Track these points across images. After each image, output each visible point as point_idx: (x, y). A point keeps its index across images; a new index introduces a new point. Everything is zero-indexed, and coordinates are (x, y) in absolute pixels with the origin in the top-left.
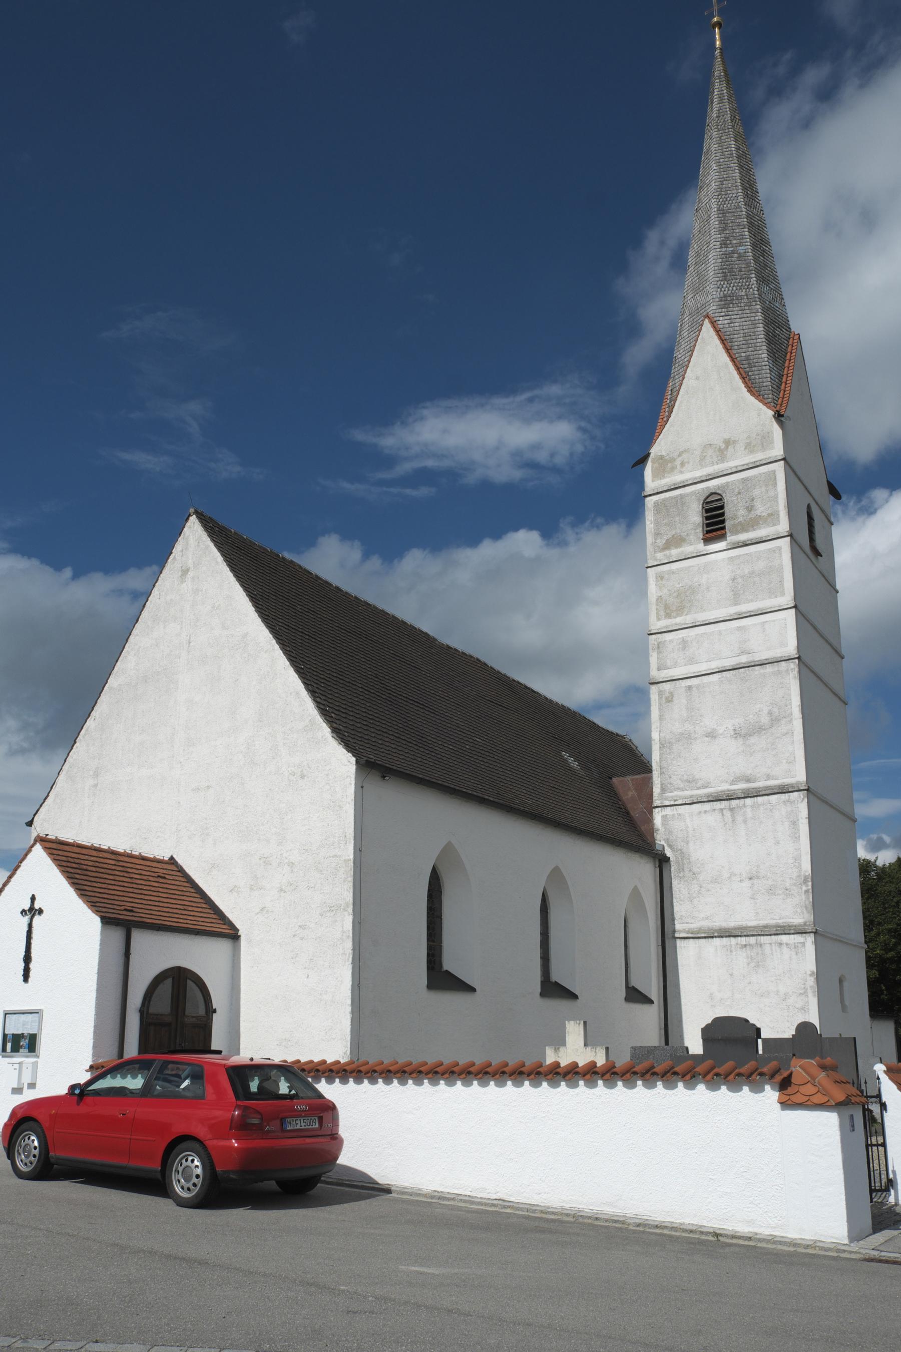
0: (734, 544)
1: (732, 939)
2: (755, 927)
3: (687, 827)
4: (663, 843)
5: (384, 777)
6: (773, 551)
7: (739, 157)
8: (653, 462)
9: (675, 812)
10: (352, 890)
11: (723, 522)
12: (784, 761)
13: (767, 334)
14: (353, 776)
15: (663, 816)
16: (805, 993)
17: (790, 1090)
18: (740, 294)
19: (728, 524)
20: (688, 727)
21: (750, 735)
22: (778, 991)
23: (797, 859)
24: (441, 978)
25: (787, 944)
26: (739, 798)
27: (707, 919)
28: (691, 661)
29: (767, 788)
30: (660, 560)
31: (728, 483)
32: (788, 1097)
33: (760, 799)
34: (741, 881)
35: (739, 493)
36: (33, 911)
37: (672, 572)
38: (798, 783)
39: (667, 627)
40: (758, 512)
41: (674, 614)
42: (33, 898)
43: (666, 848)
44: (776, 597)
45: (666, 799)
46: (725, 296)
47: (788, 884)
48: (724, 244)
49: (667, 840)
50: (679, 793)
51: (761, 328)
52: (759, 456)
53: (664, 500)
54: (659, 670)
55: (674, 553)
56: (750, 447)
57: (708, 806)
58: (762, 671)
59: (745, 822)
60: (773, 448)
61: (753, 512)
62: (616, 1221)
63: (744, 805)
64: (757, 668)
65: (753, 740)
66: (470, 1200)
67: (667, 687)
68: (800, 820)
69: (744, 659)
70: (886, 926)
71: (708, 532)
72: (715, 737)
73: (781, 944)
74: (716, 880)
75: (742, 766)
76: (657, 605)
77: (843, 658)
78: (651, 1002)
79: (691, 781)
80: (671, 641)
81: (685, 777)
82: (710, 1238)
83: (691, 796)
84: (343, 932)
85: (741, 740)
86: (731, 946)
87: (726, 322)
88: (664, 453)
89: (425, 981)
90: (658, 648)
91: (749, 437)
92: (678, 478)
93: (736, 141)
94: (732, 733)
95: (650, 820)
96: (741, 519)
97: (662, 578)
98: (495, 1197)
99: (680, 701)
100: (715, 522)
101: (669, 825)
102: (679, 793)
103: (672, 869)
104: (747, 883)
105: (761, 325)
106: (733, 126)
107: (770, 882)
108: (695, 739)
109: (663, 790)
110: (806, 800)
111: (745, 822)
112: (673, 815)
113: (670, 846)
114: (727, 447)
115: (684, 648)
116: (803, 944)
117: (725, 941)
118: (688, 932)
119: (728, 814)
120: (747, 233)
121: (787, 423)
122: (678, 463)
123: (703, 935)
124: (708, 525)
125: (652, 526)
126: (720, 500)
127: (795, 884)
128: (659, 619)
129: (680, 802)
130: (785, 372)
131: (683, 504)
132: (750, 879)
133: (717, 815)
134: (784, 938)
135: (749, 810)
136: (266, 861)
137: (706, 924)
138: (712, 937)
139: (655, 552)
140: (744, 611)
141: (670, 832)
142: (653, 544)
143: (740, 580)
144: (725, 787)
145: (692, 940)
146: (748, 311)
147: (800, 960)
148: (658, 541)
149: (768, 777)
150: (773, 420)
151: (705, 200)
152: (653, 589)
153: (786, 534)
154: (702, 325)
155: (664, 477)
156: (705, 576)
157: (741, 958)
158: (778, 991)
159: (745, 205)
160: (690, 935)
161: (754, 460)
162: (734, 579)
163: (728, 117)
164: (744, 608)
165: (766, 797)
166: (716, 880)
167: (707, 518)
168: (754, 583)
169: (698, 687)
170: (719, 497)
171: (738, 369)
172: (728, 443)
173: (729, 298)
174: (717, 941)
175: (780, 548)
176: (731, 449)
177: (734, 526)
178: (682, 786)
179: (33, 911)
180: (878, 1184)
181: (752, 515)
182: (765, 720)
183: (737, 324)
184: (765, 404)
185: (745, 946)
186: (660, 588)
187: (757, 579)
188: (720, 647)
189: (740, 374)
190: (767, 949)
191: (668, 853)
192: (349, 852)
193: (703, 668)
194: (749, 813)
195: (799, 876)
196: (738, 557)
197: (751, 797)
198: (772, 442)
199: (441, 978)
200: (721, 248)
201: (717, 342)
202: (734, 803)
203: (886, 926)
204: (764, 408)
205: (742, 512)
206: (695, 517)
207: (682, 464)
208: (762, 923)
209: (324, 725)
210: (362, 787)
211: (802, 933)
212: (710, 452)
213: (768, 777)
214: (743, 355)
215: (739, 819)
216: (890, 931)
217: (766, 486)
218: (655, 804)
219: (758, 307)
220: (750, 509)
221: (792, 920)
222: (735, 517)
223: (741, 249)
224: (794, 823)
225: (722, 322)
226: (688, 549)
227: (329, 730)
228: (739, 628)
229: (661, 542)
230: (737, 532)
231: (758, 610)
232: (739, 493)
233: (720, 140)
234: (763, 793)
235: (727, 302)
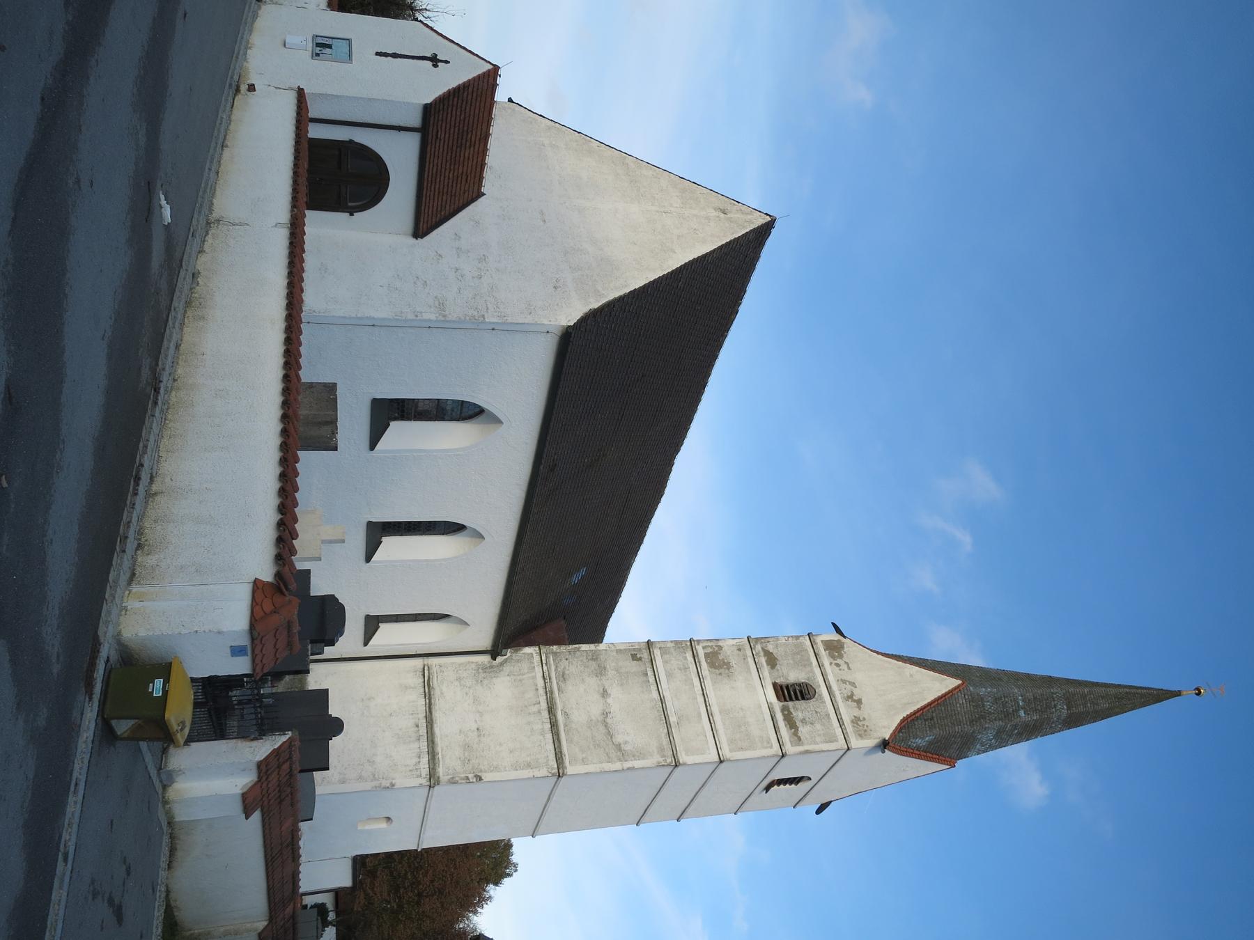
6: (769, 741)
11: (791, 699)
19: (790, 704)
20: (611, 673)
23: (497, 769)
24: (378, 532)
28: (669, 675)
36: (434, 60)
42: (446, 62)
50: (553, 668)
56: (856, 721)
69: (673, 719)
75: (578, 717)
79: (563, 677)
80: (685, 658)
82: (146, 373)
92: (826, 661)
95: (530, 644)
99: (634, 666)
102: (553, 668)
104: (474, 727)
109: (555, 654)
111: (529, 723)
113: (506, 661)
119: (535, 709)
122: (839, 661)
134: (425, 759)
136: (483, 259)
144: (559, 706)
172: (859, 702)
179: (434, 60)
181: (799, 724)
182: (619, 738)
190: (416, 745)
191: (499, 659)
199: (378, 532)
202: (546, 714)
205: (800, 715)
206: (793, 676)
207: (838, 665)
220: (803, 721)
223: (1022, 713)
226: (766, 670)
228: (699, 715)
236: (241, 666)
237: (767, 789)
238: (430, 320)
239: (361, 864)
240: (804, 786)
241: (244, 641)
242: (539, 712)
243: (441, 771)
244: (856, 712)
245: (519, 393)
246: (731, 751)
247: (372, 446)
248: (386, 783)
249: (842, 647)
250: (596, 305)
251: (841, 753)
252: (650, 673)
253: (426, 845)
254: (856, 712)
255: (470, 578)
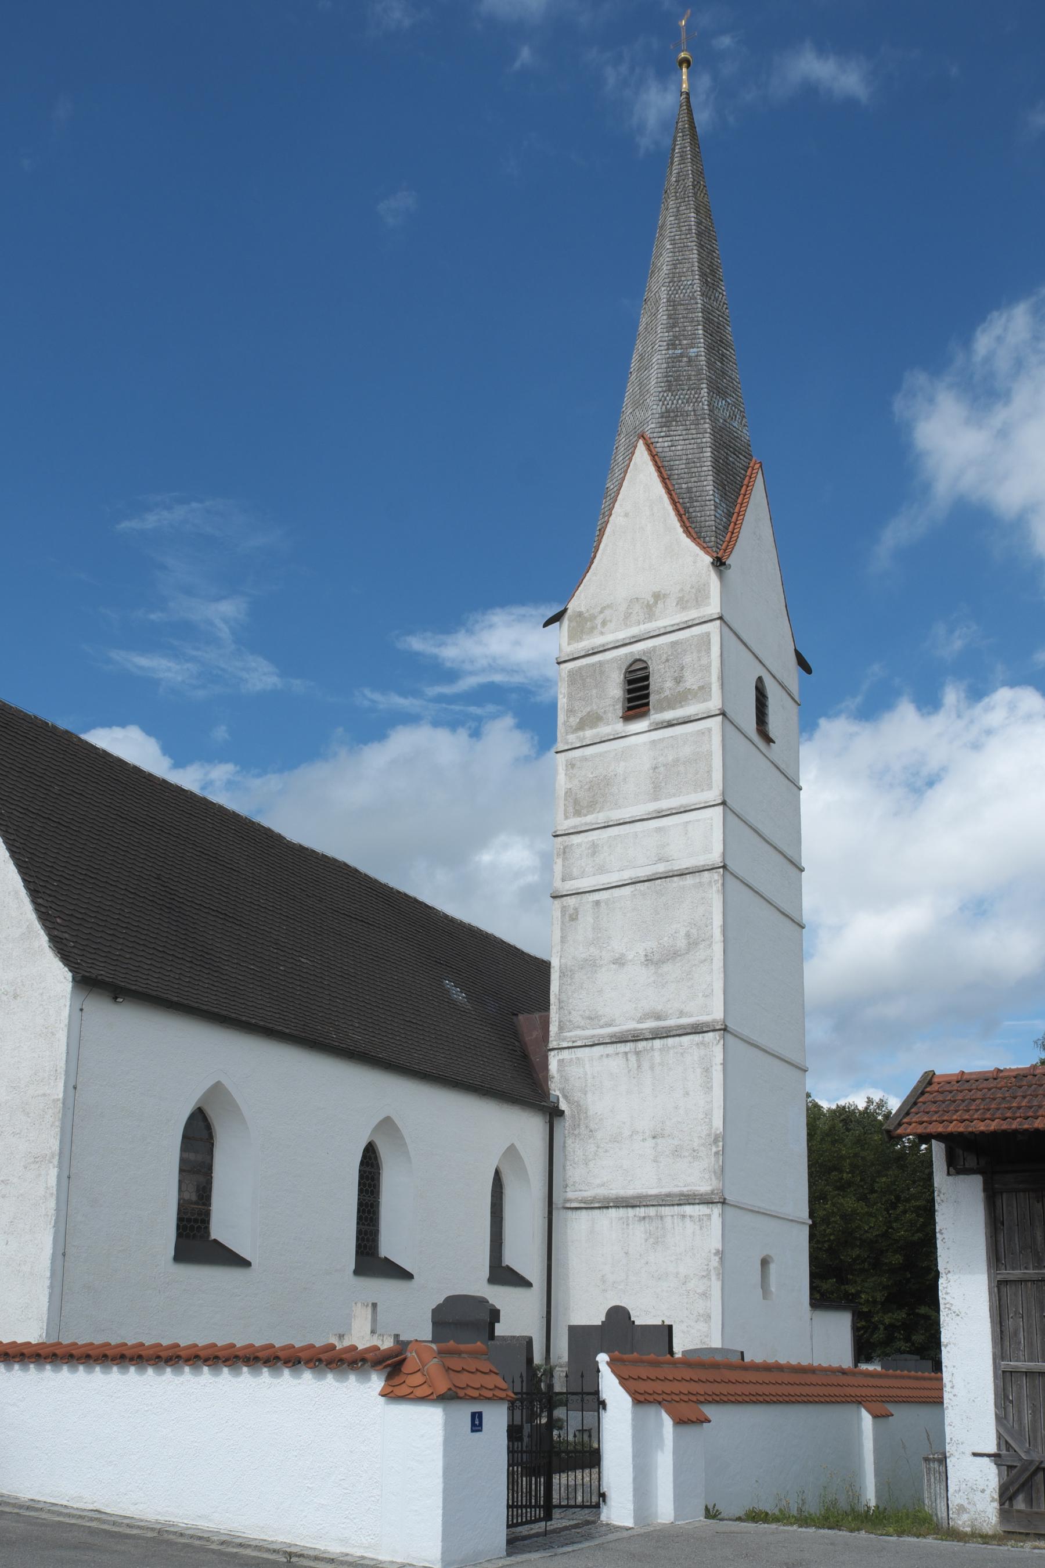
0: (657, 724)
1: (630, 1210)
2: (656, 1196)
3: (586, 1074)
4: (557, 1093)
5: (115, 998)
6: (701, 733)
7: (699, 234)
8: (570, 621)
9: (573, 1056)
10: (58, 1137)
11: (647, 696)
12: (701, 995)
13: (716, 460)
14: (69, 996)
15: (559, 1061)
16: (707, 1276)
17: (397, 1380)
18: (686, 409)
19: (653, 699)
21: (663, 962)
22: (677, 1273)
23: (708, 1114)
25: (691, 1217)
26: (647, 1039)
27: (603, 1185)
28: (602, 870)
29: (679, 1027)
30: (572, 743)
31: (655, 647)
32: (391, 1389)
33: (670, 1041)
34: (644, 1140)
35: (667, 660)
37: (585, 759)
38: (715, 1021)
39: (575, 827)
40: (688, 685)
41: (584, 811)
43: (561, 1099)
44: (702, 790)
45: (564, 1040)
46: (668, 411)
47: (695, 1144)
48: (672, 345)
49: (562, 1090)
50: (579, 1032)
51: (708, 453)
52: (693, 614)
53: (580, 668)
54: (563, 880)
55: (589, 734)
56: (682, 603)
57: (610, 1049)
58: (681, 883)
59: (652, 1068)
60: (709, 604)
61: (681, 684)
62: (200, 1538)
63: (652, 1049)
64: (675, 878)
65: (666, 968)
66: (52, 1509)
67: (571, 901)
68: (714, 1067)
69: (661, 868)
70: (914, 1203)
71: (630, 709)
72: (623, 964)
73: (684, 1216)
74: (615, 1139)
76: (565, 800)
77: (802, 870)
78: (527, 1284)
79: (593, 1019)
80: (579, 845)
81: (587, 1013)
83: (593, 1036)
84: (47, 1188)
85: (652, 968)
86: (628, 1218)
87: (666, 444)
88: (583, 609)
89: (352, 1266)
90: (564, 852)
91: (682, 590)
93: (697, 212)
94: (643, 959)
96: (667, 693)
97: (573, 766)
98: (91, 1507)
99: (587, 919)
100: (638, 695)
101: (568, 1069)
102: (579, 1032)
103: (567, 1124)
104: (650, 1142)
105: (709, 449)
106: (695, 194)
107: (676, 1142)
108: (601, 966)
109: (561, 1028)
110: (722, 1042)
111: (652, 1068)
112: (571, 1059)
113: (565, 1097)
114: (656, 603)
115: (594, 854)
116: (709, 1216)
117: (622, 1212)
118: (581, 1201)
119: (633, 1058)
120: (701, 332)
121: (730, 573)
122: (599, 621)
123: (597, 1205)
124: (630, 700)
125: (565, 700)
126: (646, 668)
127: (703, 1145)
128: (566, 818)
129: (579, 1043)
130: (737, 510)
131: (602, 673)
132: (654, 1138)
133: (620, 1061)
134: (688, 1209)
135: (656, 1054)
137: (602, 1192)
138: (607, 1207)
139: (567, 734)
140: (664, 808)
141: (567, 1080)
142: (564, 723)
143: (662, 769)
144: (632, 1025)
145: (584, 1212)
146: (694, 432)
147: (700, 1235)
148: (571, 719)
149: (682, 1014)
150: (711, 568)
151: (654, 289)
152: (562, 782)
153: (718, 712)
154: (635, 447)
155: (581, 639)
156: (622, 764)
157: (639, 1232)
158: (677, 1273)
159: (703, 295)
160: (583, 1205)
161: (686, 619)
162: (655, 768)
163: (689, 182)
164: (665, 804)
165: (677, 1039)
166: (615, 1139)
167: (629, 691)
168: (678, 773)
169: (607, 902)
170: (645, 665)
171: (674, 503)
172: (657, 597)
173: (672, 414)
174: (612, 1212)
175: (710, 730)
176: (660, 605)
177: (659, 701)
178: (582, 1024)
180: (579, 1499)
181: (681, 688)
182: (681, 943)
183: (679, 448)
184: (703, 548)
185: (644, 1218)
186: (570, 777)
187: (682, 768)
188: (631, 853)
189: (676, 509)
190: (668, 1221)
191: (563, 1106)
192: (58, 1090)
193: (614, 878)
194: (657, 1057)
195: (709, 1135)
196: (662, 740)
197: (660, 1038)
198: (708, 597)
200: (668, 349)
201: (651, 468)
202: (641, 1045)
203: (914, 1203)
204: (701, 553)
205: (669, 684)
206: (615, 690)
207: (604, 623)
208: (664, 1190)
209: (42, 932)
210: (81, 1010)
211: (708, 1203)
212: (637, 608)
213: (682, 1014)
214: (684, 486)
215: (646, 1065)
216: (918, 1208)
217: (699, 651)
218: (551, 1046)
219: (707, 426)
220: (678, 680)
221: (697, 1188)
222: (661, 690)
223: (693, 352)
224: (707, 1070)
225: (662, 444)
226: (604, 730)
227: (46, 938)
228: (659, 830)
229: (574, 721)
230: (662, 710)
231: (681, 806)
232: (667, 660)
233: (678, 211)
234: (674, 1033)
235: (669, 418)
236: (497, 1419)
237: (769, 740)
238: (59, 1177)
239: (823, 1296)
240: (772, 689)
241: (464, 1412)
242: (637, 1053)
243: (704, 1187)
244: (672, 602)
245: (180, 1059)
246: (710, 787)
247: (245, 1263)
248: (715, 1261)
249: (580, 614)
250: (43, 939)
251: (726, 629)
252: (596, 896)
253: (801, 1209)
254: (672, 602)
255: (451, 1141)
